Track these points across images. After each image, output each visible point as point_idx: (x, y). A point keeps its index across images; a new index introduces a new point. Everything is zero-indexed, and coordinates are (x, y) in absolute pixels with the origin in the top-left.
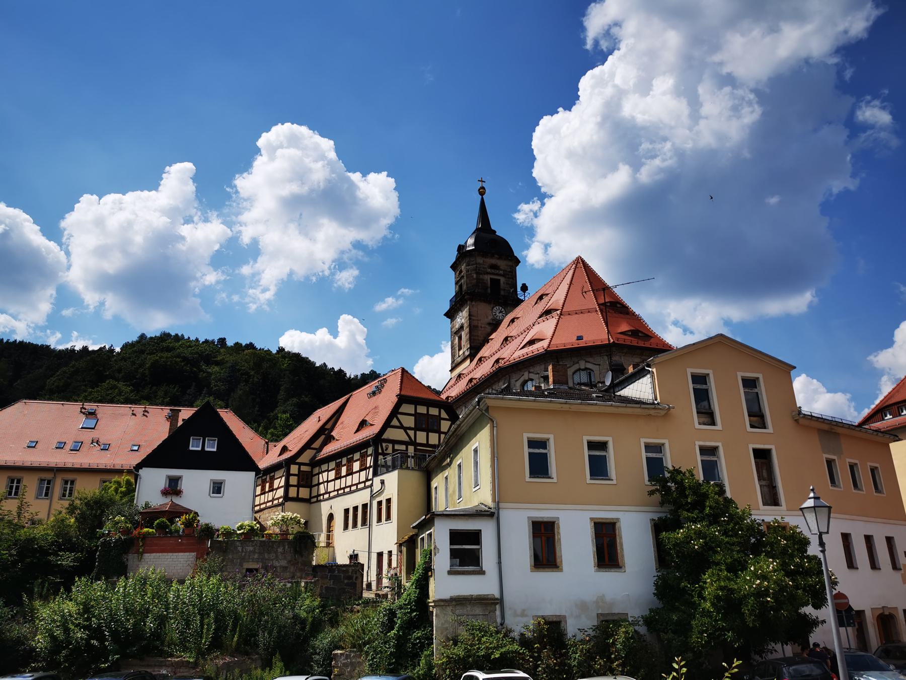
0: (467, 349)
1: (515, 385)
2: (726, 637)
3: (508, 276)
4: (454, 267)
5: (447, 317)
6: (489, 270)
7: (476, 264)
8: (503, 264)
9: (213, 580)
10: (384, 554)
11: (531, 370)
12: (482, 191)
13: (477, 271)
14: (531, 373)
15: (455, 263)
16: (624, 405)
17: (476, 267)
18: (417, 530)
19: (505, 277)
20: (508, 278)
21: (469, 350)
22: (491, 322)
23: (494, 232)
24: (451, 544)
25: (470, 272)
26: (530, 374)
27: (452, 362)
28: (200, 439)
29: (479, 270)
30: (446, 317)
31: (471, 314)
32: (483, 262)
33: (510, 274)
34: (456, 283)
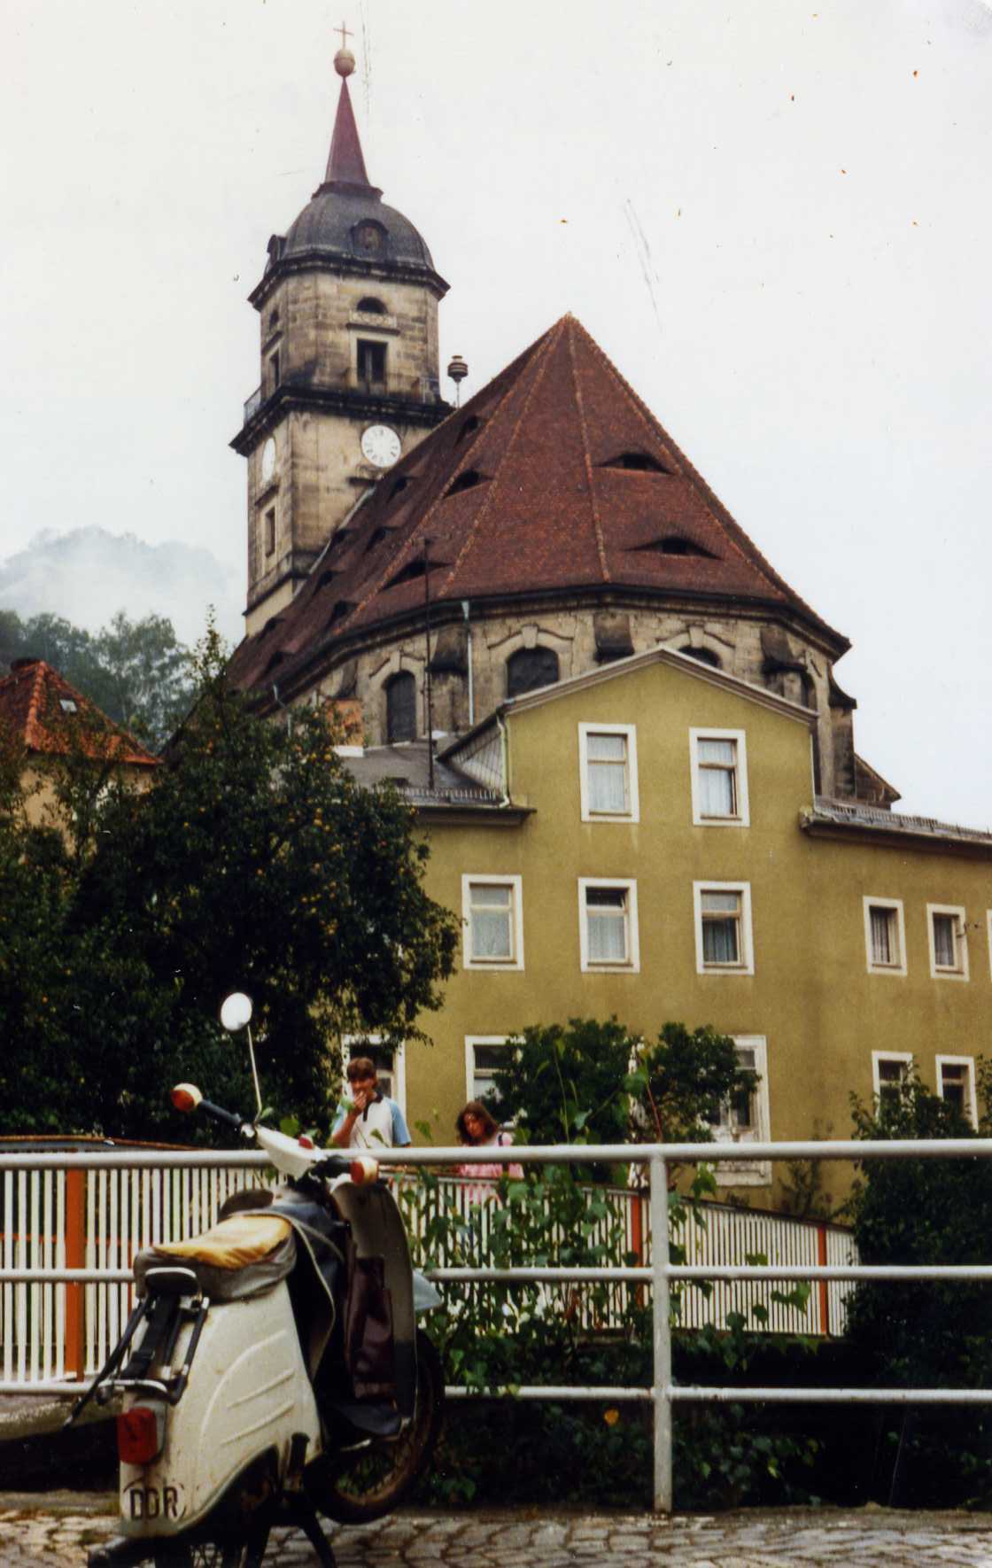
0: (287, 556)
1: (368, 686)
2: (167, 942)
3: (409, 333)
4: (259, 298)
5: (238, 452)
6: (355, 317)
7: (317, 298)
8: (399, 298)
9: (129, 961)
10: (422, 578)
11: (408, 649)
12: (344, 68)
13: (320, 317)
14: (407, 655)
15: (260, 288)
16: (723, 611)
17: (317, 306)
18: (228, 656)
19: (404, 337)
20: (412, 339)
21: (291, 558)
22: (358, 475)
23: (375, 193)
24: (642, 1502)
25: (298, 322)
26: (404, 659)
27: (252, 589)
28: (590, 964)
29: (325, 316)
30: (234, 451)
31: (298, 450)
32: (339, 292)
33: (418, 325)
34: (264, 351)
